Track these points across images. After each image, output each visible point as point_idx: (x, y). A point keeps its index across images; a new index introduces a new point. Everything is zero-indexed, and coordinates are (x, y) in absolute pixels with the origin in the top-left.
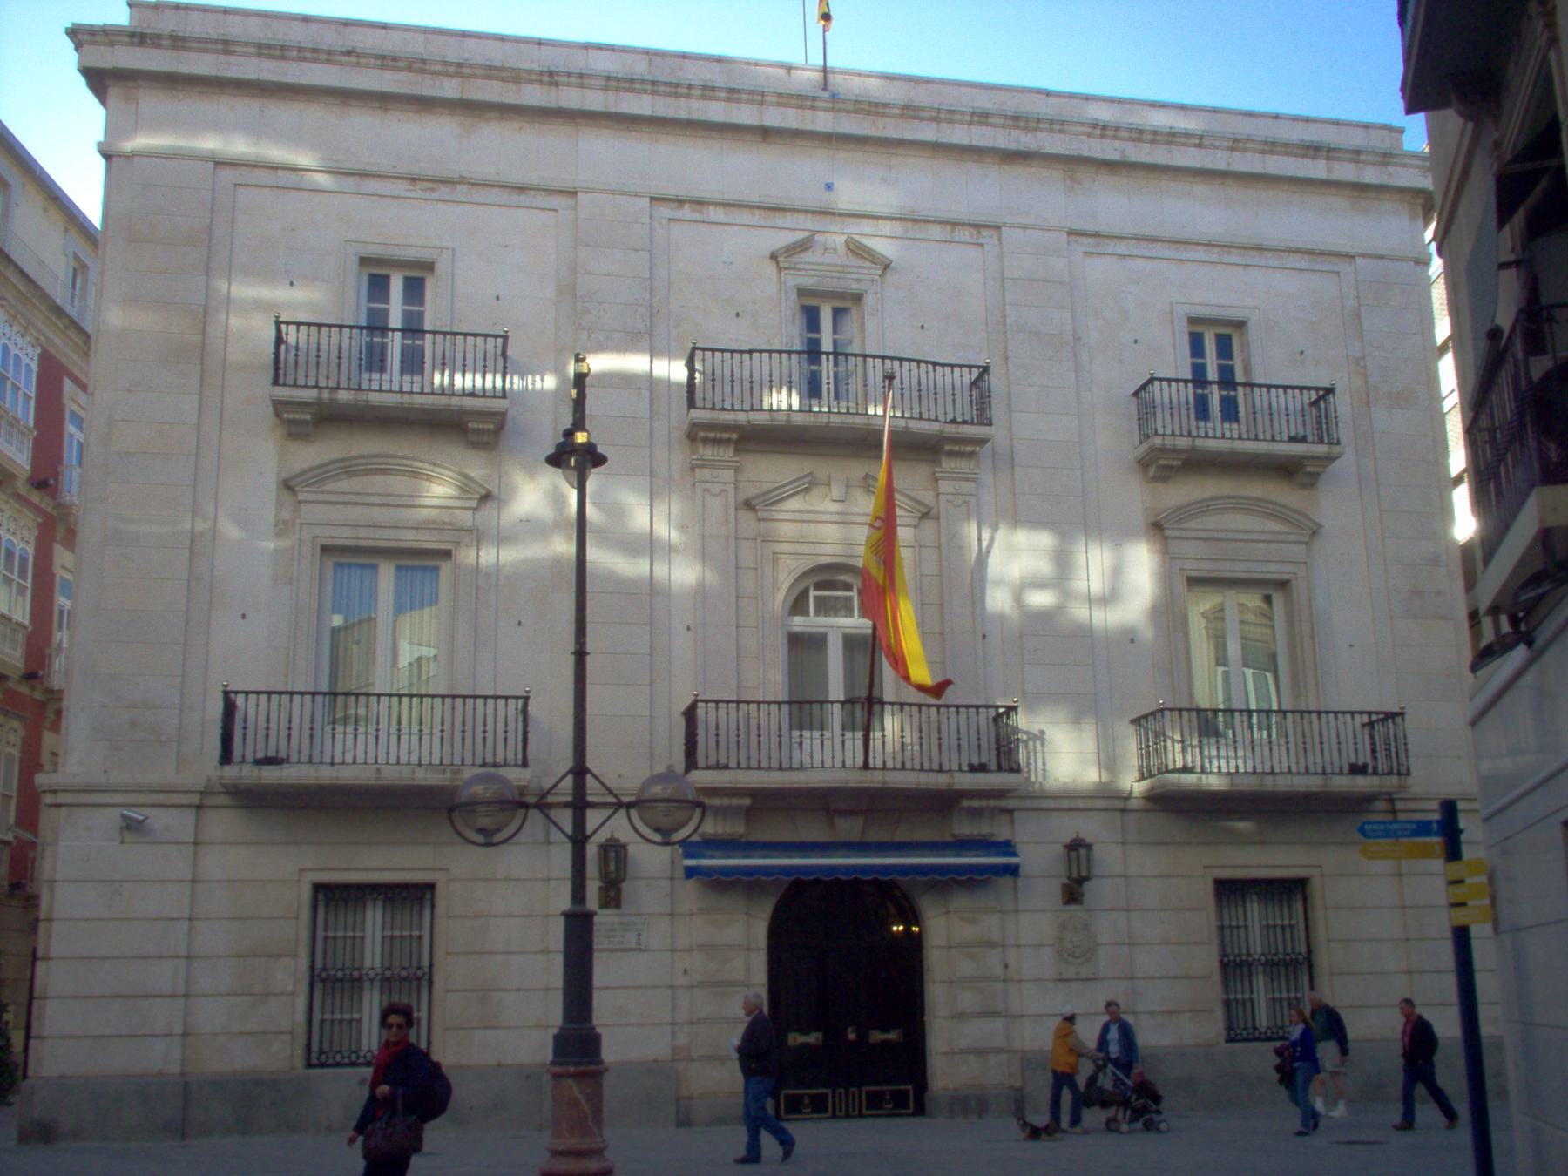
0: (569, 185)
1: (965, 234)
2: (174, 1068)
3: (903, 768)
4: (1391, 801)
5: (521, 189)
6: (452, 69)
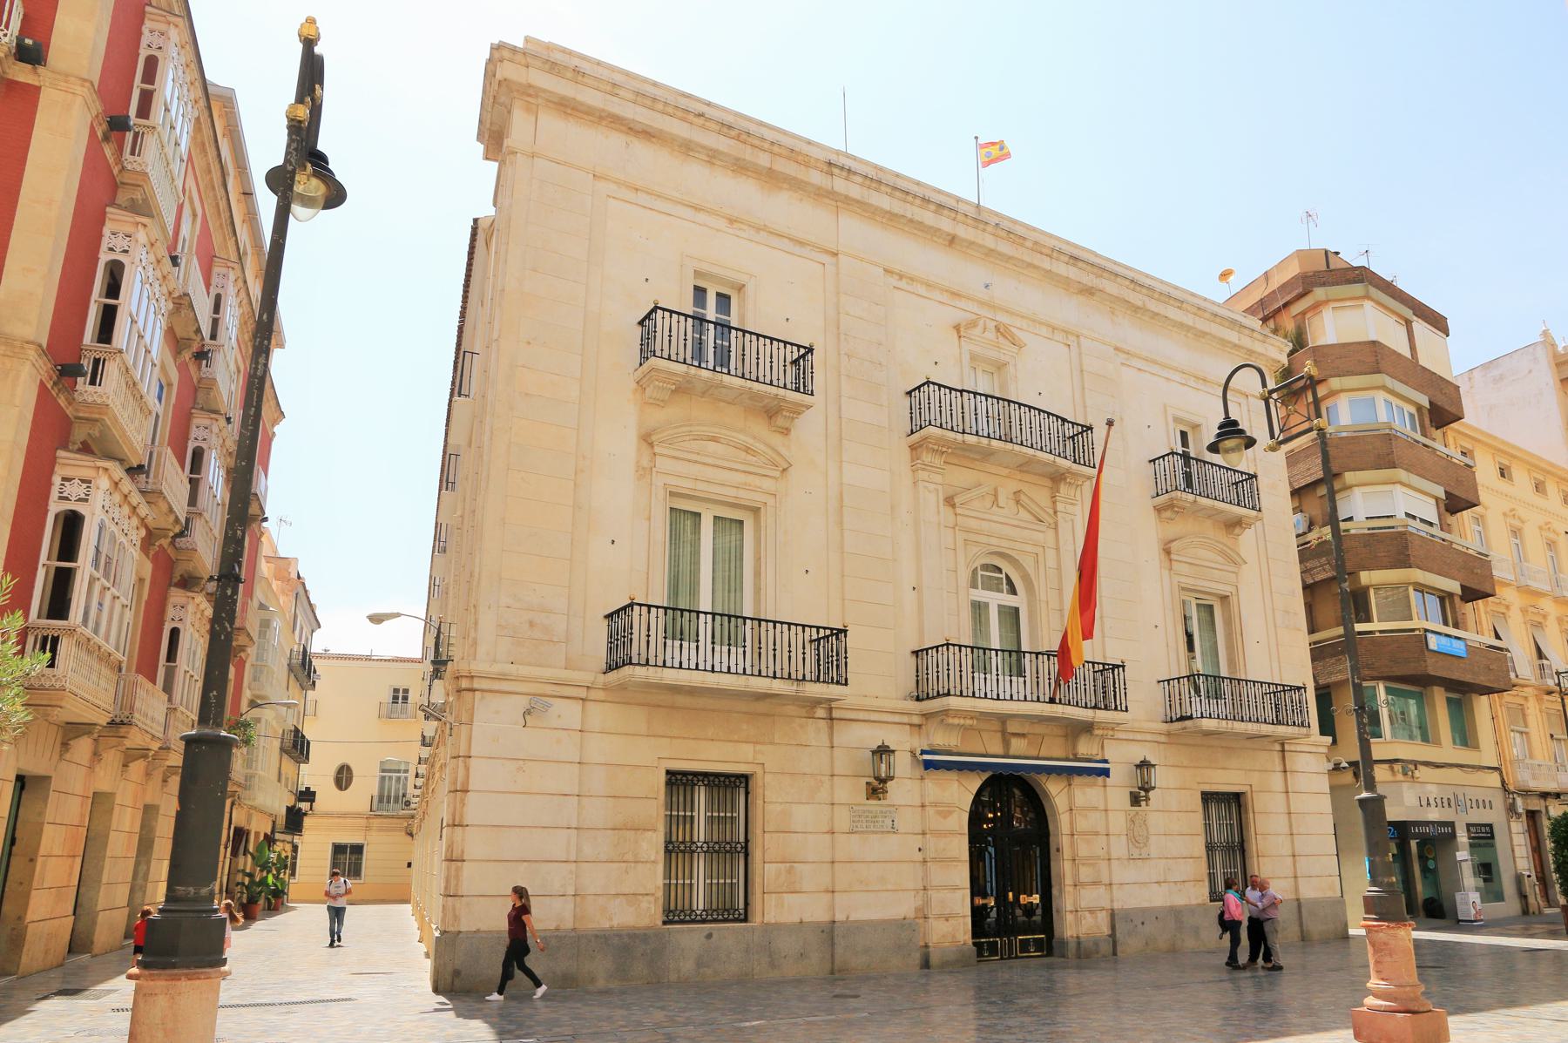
0: (833, 247)
1: (1059, 336)
3: (647, 663)
4: (1283, 745)
5: (801, 243)
6: (766, 146)
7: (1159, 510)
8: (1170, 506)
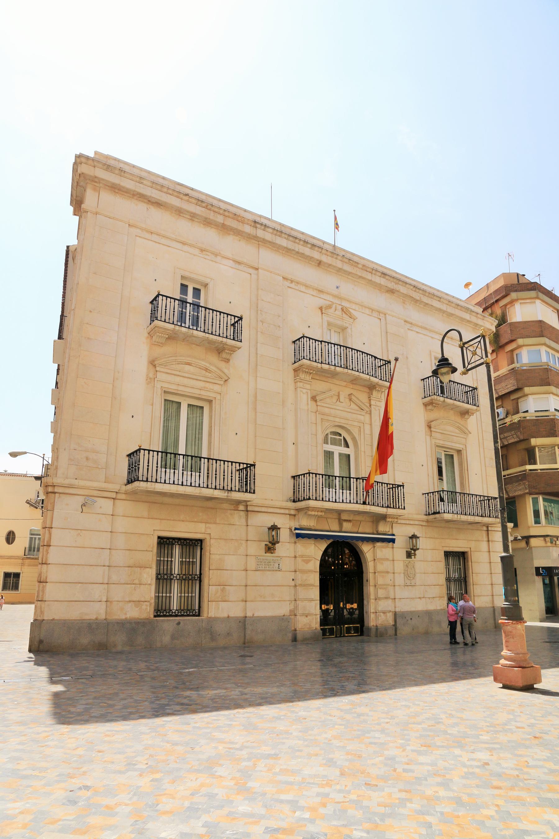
0: (256, 266)
2: (103, 616)
4: (488, 527)
6: (221, 212)
7: (426, 405)
8: (431, 403)
